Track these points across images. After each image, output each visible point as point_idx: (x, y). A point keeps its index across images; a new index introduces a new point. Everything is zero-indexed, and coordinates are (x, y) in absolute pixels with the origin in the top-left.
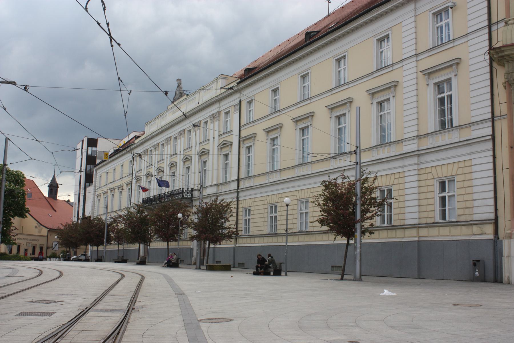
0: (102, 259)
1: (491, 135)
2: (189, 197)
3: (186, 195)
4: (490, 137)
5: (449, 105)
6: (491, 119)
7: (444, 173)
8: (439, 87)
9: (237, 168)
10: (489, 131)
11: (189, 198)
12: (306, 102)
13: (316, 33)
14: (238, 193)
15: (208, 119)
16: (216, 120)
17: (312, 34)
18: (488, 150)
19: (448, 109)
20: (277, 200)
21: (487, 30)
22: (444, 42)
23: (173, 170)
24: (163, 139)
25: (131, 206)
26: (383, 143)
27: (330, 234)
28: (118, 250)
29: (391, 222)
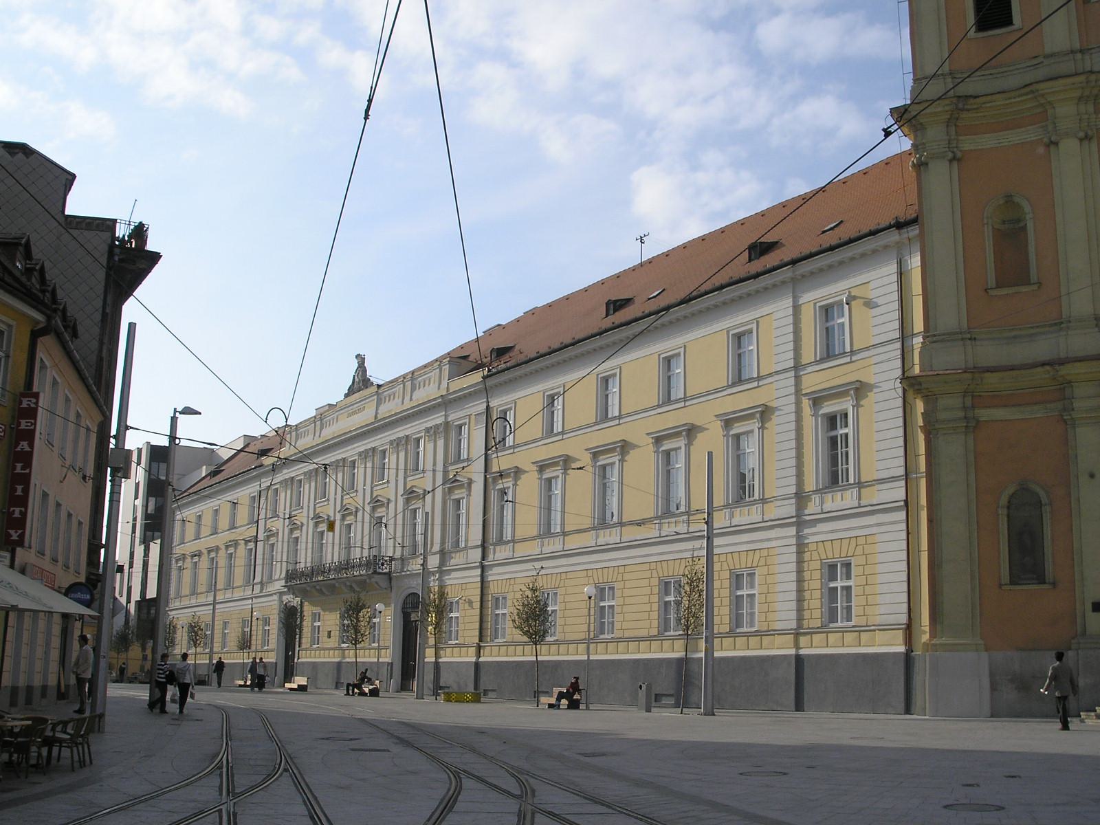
0: (207, 679)
1: (904, 501)
2: (385, 571)
3: (379, 568)
4: (902, 503)
5: (844, 450)
6: (904, 477)
7: (835, 554)
8: (832, 421)
9: (481, 527)
10: (901, 494)
11: (385, 574)
12: (676, 404)
13: (624, 302)
14: (709, 539)
15: (302, 477)
16: (439, 437)
17: (618, 303)
18: (900, 522)
19: (842, 454)
20: (558, 582)
21: (899, 345)
22: (837, 353)
23: (322, 527)
24: (302, 471)
25: (255, 582)
26: (602, 523)
27: (130, 648)
28: (477, 665)
29: (849, 619)
